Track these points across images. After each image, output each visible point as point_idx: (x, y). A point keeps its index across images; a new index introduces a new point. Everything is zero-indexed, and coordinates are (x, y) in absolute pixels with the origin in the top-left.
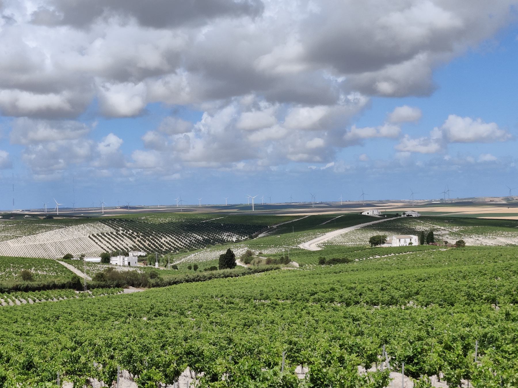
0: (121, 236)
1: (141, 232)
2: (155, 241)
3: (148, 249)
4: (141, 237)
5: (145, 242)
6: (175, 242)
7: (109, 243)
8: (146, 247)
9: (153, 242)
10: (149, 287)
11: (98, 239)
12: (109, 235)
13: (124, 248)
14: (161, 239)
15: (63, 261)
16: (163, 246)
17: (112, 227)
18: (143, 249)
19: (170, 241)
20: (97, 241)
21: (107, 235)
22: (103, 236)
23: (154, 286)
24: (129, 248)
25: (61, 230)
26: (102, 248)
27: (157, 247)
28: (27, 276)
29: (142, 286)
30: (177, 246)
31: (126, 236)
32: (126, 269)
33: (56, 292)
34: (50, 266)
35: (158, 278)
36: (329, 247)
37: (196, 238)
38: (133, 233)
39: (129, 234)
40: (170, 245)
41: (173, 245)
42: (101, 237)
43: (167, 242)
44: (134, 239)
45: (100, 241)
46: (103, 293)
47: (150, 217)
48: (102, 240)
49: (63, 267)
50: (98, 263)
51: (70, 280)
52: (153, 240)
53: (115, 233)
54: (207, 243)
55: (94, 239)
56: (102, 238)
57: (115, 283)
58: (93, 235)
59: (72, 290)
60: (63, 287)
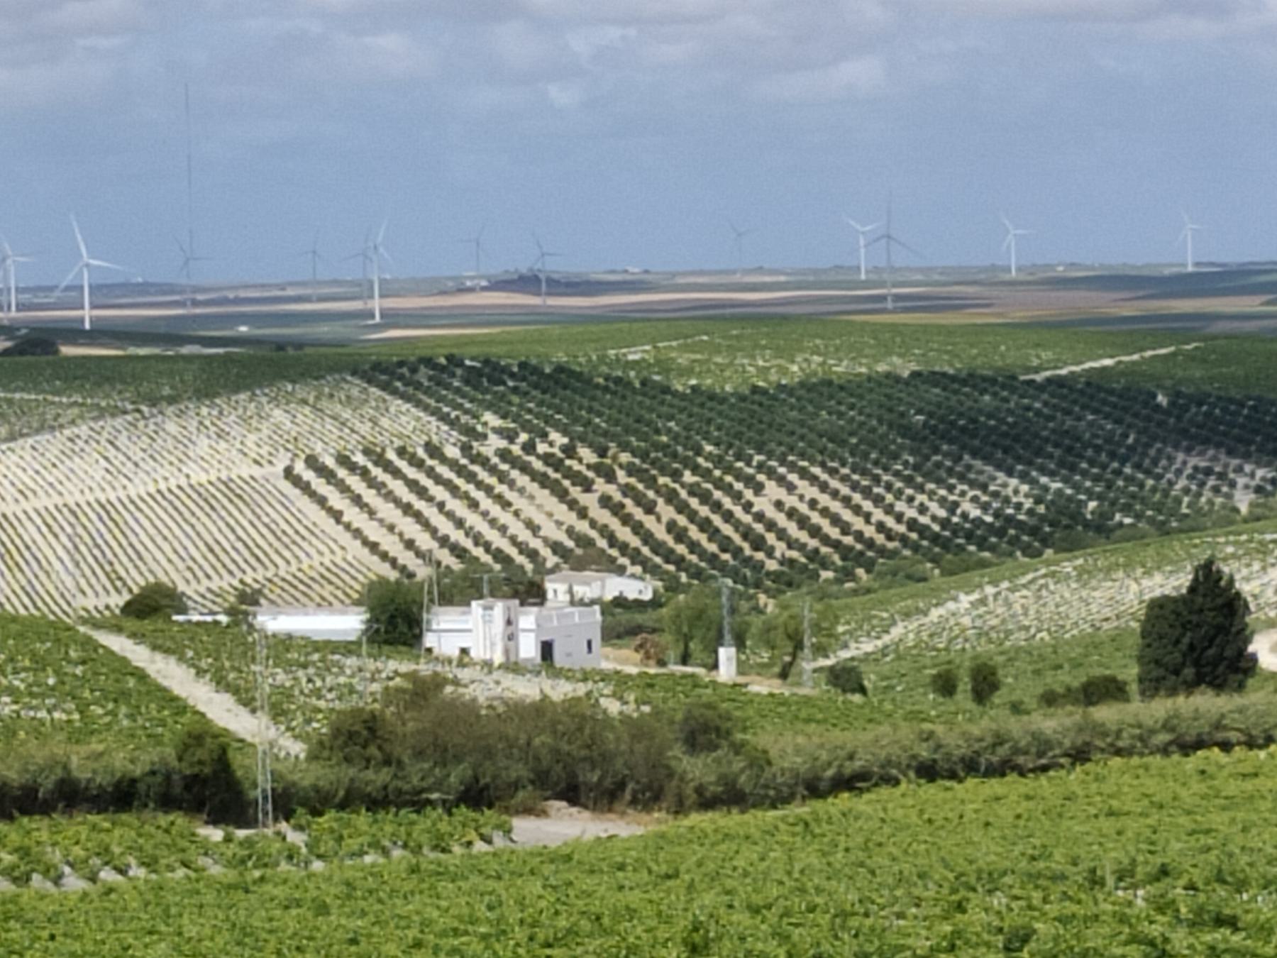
0: (493, 470)
1: (624, 447)
2: (717, 507)
3: (669, 556)
4: (622, 476)
5: (650, 509)
6: (847, 515)
7: (418, 516)
8: (658, 547)
9: (704, 511)
10: (680, 809)
11: (344, 488)
12: (418, 463)
14: (758, 489)
15: (118, 629)
16: (771, 538)
17: (435, 412)
18: (636, 557)
19: (813, 504)
20: (336, 500)
21: (402, 465)
22: (376, 472)
23: (707, 803)
24: (545, 552)
25: (109, 424)
26: (373, 547)
29: (634, 802)
30: (859, 536)
31: (525, 469)
32: (527, 689)
34: (40, 664)
35: (738, 749)
38: (569, 451)
39: (547, 459)
40: (815, 532)
41: (834, 533)
42: (364, 473)
43: (791, 513)
44: (575, 492)
45: (357, 500)
47: (685, 348)
48: (369, 496)
49: (124, 667)
50: (348, 648)
51: (170, 752)
52: (705, 498)
53: (452, 452)
54: (1059, 531)
55: (320, 485)
56: (372, 483)
57: (457, 776)
58: (312, 462)
59: (180, 820)
60: (122, 797)
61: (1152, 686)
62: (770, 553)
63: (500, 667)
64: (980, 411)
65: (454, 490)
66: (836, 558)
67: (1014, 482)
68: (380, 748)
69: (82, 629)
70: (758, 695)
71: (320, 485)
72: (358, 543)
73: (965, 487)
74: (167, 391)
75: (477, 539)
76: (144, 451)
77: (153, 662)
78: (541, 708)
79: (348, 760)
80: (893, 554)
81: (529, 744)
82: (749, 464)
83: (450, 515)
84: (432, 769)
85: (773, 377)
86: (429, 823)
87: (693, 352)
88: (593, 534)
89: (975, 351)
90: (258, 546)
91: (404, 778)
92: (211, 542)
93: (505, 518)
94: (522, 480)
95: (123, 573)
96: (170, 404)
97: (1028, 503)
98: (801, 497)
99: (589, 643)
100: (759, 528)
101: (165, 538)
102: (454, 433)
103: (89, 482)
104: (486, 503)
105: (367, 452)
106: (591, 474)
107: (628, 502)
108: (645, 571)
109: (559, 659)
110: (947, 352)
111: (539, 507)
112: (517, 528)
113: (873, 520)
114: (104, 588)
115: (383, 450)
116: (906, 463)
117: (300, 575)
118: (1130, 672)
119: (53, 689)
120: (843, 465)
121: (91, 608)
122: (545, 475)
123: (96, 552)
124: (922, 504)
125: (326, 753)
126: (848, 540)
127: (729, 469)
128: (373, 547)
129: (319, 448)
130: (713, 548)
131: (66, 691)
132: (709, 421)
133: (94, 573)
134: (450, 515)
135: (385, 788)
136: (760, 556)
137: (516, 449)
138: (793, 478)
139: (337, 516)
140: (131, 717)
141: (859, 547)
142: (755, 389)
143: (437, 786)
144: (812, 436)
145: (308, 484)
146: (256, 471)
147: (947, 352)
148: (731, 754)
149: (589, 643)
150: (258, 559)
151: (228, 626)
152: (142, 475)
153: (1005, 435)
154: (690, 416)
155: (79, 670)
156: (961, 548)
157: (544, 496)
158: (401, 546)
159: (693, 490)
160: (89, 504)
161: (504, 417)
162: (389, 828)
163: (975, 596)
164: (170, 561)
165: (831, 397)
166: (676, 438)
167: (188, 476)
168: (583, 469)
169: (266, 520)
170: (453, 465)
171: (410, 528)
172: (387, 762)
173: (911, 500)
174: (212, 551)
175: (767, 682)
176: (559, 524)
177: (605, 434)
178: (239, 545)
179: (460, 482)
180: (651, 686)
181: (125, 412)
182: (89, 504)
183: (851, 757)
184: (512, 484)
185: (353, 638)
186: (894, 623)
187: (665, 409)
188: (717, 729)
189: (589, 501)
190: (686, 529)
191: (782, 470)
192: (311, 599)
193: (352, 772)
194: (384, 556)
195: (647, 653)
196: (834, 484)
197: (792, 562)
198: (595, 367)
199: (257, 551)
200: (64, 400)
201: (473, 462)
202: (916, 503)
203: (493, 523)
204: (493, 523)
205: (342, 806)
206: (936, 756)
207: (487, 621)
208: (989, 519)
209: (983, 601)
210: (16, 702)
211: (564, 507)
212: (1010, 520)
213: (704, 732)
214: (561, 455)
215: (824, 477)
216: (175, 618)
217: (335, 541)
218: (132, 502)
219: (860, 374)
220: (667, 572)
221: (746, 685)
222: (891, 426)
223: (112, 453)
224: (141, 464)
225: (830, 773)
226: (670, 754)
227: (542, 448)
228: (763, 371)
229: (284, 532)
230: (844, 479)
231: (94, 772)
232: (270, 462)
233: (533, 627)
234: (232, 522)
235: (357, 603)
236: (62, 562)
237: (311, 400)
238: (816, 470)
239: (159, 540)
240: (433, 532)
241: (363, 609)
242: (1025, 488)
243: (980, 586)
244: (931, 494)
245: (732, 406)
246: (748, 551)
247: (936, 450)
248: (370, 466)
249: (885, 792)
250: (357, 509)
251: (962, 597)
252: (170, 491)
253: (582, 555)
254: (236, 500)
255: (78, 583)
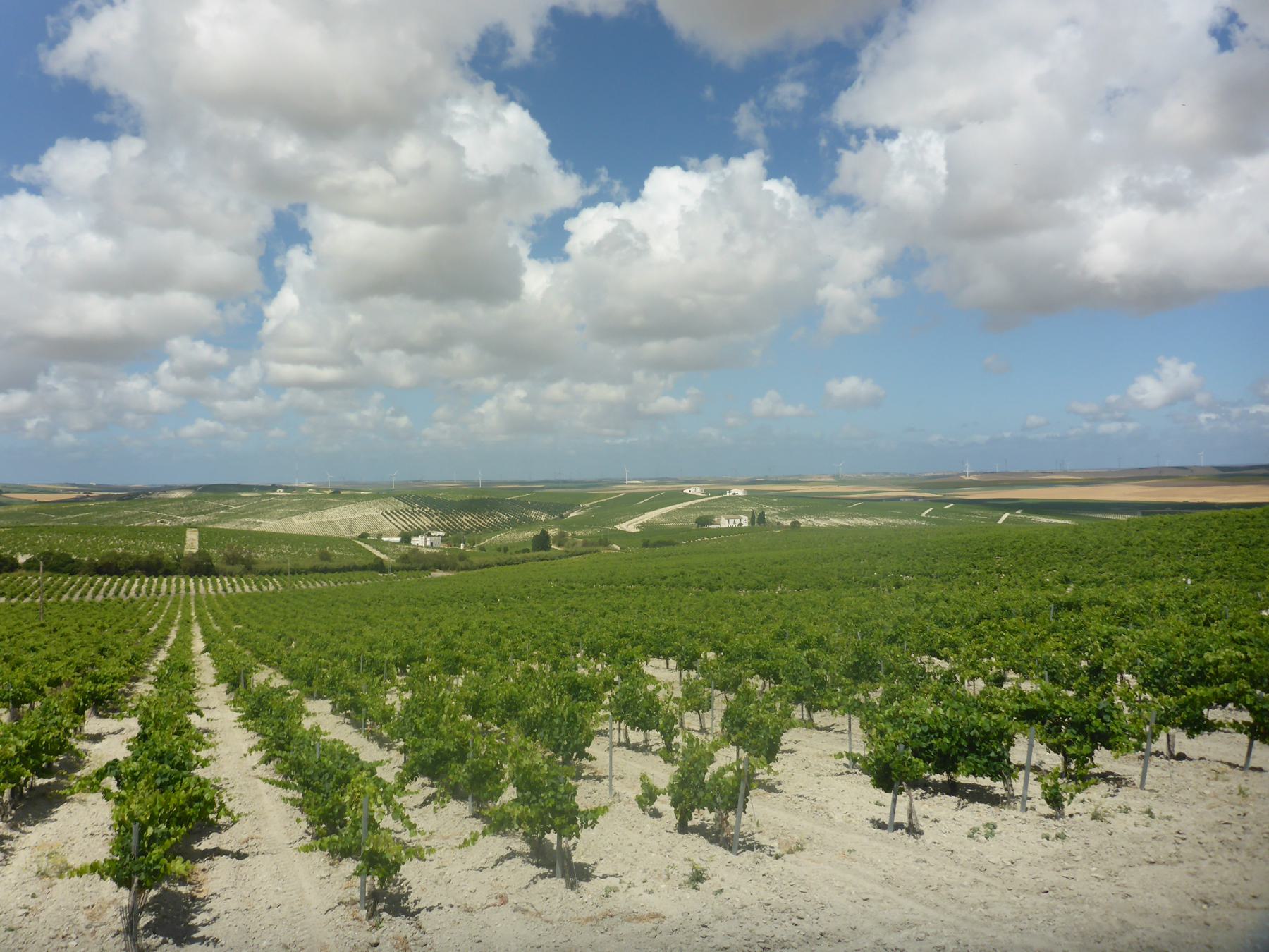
28: (325, 556)
36: (648, 528)
54: (513, 524)
60: (364, 568)
61: (534, 550)
118: (530, 548)
131: (351, 550)
173: (379, 806)
213: (462, 557)
253: (433, 528)
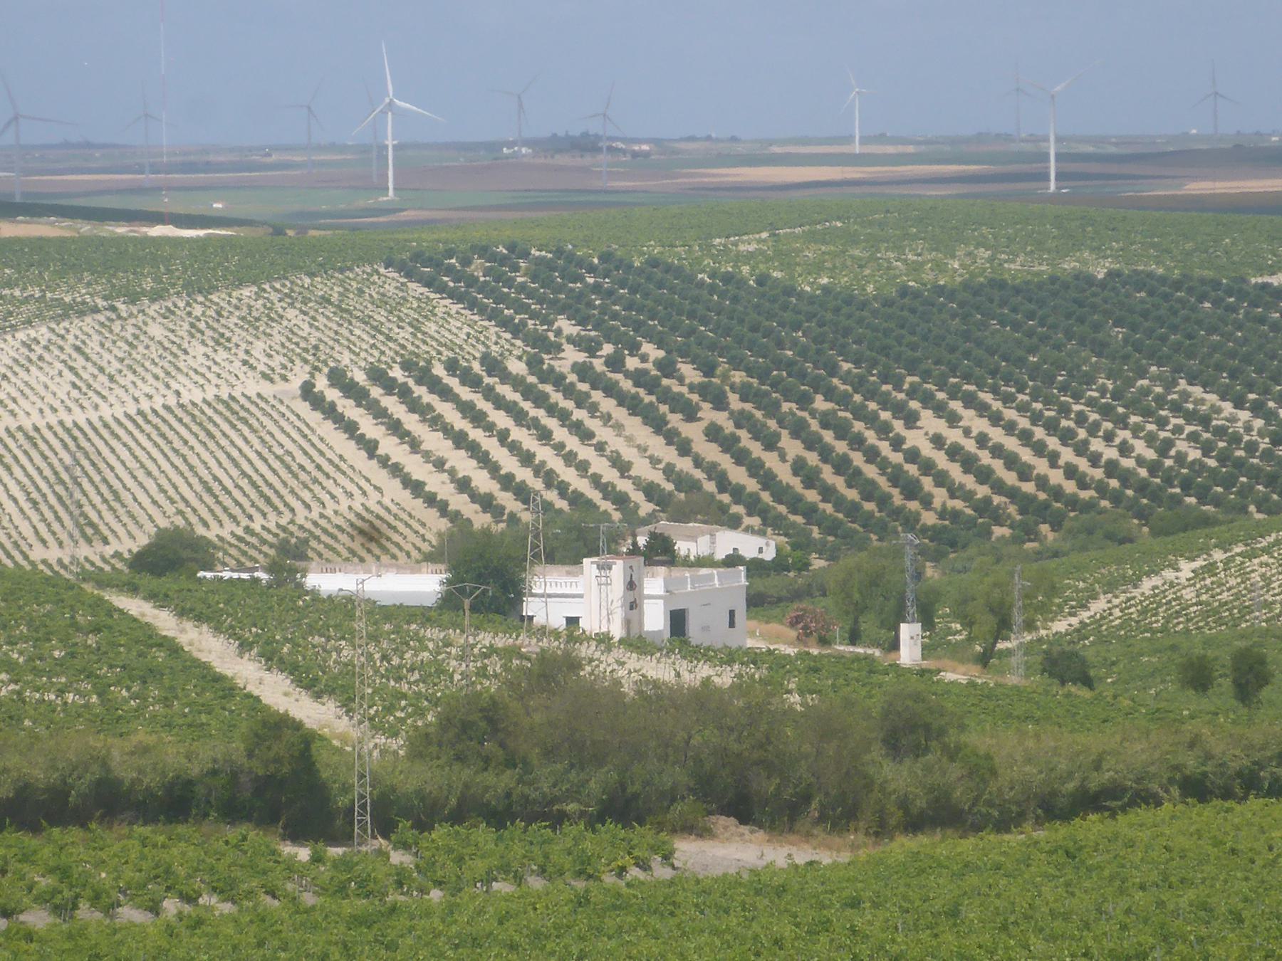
0: (569, 391)
1: (736, 363)
2: (857, 442)
3: (795, 504)
4: (734, 401)
5: (771, 444)
6: (1026, 455)
7: (474, 450)
8: (781, 493)
9: (841, 447)
10: (881, 831)
11: (379, 413)
12: (472, 381)
13: (595, 495)
14: (911, 420)
15: (133, 589)
16: (927, 483)
17: (493, 315)
18: (754, 506)
19: (982, 440)
20: (369, 427)
21: (453, 383)
22: (420, 391)
23: (914, 825)
24: (637, 497)
25: (75, 328)
26: (416, 487)
27: (869, 491)
29: (822, 819)
30: (1042, 482)
31: (611, 390)
32: (660, 670)
33: (117, 851)
34: (41, 633)
35: (953, 754)
37: (1205, 421)
38: (667, 368)
39: (639, 378)
40: (984, 475)
41: (1010, 478)
42: (404, 394)
43: (955, 453)
44: (675, 420)
45: (396, 428)
46: (505, 869)
47: (812, 237)
48: (411, 422)
49: (149, 637)
50: (421, 615)
51: (238, 747)
52: (842, 432)
53: (517, 367)
55: (348, 408)
56: (415, 406)
57: (598, 782)
58: (338, 378)
59: (254, 835)
60: (175, 803)
62: (927, 503)
63: (621, 641)
64: (1199, 323)
65: (519, 417)
66: (1012, 509)
67: (1244, 415)
68: (502, 745)
69: (88, 587)
70: (953, 683)
71: (348, 408)
72: (397, 483)
73: (1180, 421)
74: (148, 284)
75: (550, 479)
76: (122, 360)
77: (183, 631)
78: (704, 695)
79: (460, 758)
80: (1089, 506)
81: (687, 743)
82: (898, 388)
83: (514, 448)
84: (567, 771)
85: (928, 276)
86: (569, 843)
87: (824, 242)
88: (699, 474)
89: (1189, 246)
90: (270, 486)
91: (530, 784)
92: (209, 478)
93: (586, 453)
94: (607, 404)
95: (93, 516)
96: (153, 300)
97: (1264, 444)
98: (967, 432)
99: (732, 613)
100: (912, 469)
101: (149, 474)
102: (519, 343)
103: (49, 398)
104: (560, 434)
105: (407, 366)
106: (695, 398)
107: (743, 434)
108: (765, 523)
109: (695, 633)
110: (1153, 245)
111: (629, 439)
112: (600, 466)
113: (1061, 462)
114: (71, 536)
115: (429, 362)
116: (1103, 391)
117: (323, 522)
119: (59, 663)
120: (1021, 391)
121: (53, 562)
122: (636, 397)
123: (59, 489)
124: (1124, 442)
125: (434, 749)
126: (1029, 487)
127: (871, 394)
128: (416, 487)
129: (346, 359)
130: (852, 495)
132: (847, 332)
133: (58, 518)
134: (514, 448)
135: (508, 795)
136: (914, 505)
137: (599, 365)
138: (956, 405)
139: (370, 448)
140: (166, 702)
141: (1042, 496)
142: (904, 291)
143: (570, 796)
144: (980, 352)
145: (333, 405)
146: (267, 389)
147: (1153, 245)
148: (945, 760)
149: (732, 613)
150: (268, 500)
151: (270, 586)
152: (121, 392)
153: (1232, 355)
154: (821, 324)
155: (92, 640)
156: (1176, 500)
157: (634, 425)
158: (451, 487)
159: (827, 421)
160: (50, 428)
161: (582, 322)
162: (518, 849)
163: (1199, 563)
164: (155, 502)
165: (1003, 303)
166: (803, 353)
167: (178, 393)
168: (684, 390)
169: (280, 452)
170: (518, 383)
171: (464, 464)
172: (510, 763)
174: (209, 490)
175: (962, 668)
176: (654, 461)
177: (713, 347)
178: (244, 483)
179: (526, 405)
180: (816, 670)
181: (96, 310)
182: (50, 428)
183: (1097, 766)
184: (593, 409)
185: (429, 602)
186: (1095, 597)
187: (787, 315)
188: (927, 727)
189: (692, 431)
190: (818, 471)
191: (941, 396)
192: (339, 555)
193: (467, 774)
194: (431, 500)
195: (805, 628)
196: (1010, 414)
197: (955, 515)
198: (698, 261)
199: (266, 490)
200: (17, 293)
201: (543, 380)
202: (1117, 441)
203: (570, 458)
204: (570, 458)
205: (457, 817)
206: (1208, 769)
207: (604, 583)
208: (1212, 463)
209: (1210, 569)
210: (16, 682)
211: (661, 440)
212: (1240, 464)
214: (654, 372)
215: (997, 405)
216: (201, 574)
217: (368, 480)
218: (106, 426)
219: (1038, 274)
220: (794, 525)
221: (939, 671)
222: (1082, 342)
223: (80, 362)
224: (117, 377)
225: (1071, 786)
226: (867, 757)
227: (632, 363)
228: (916, 268)
229: (302, 467)
230: (1022, 409)
231: (141, 771)
232: (284, 378)
233: (661, 592)
234: (235, 454)
235: (430, 558)
236: (15, 501)
237: (335, 298)
238: (986, 397)
239: (141, 474)
240: (493, 468)
241: (443, 567)
242: (1259, 423)
243: (1206, 550)
244: (1136, 431)
245: (875, 313)
246: (898, 499)
247: (1142, 374)
248: (411, 382)
249: (1142, 814)
250: (396, 440)
251: (1183, 564)
252: (154, 411)
254: (240, 426)
255: (37, 532)
